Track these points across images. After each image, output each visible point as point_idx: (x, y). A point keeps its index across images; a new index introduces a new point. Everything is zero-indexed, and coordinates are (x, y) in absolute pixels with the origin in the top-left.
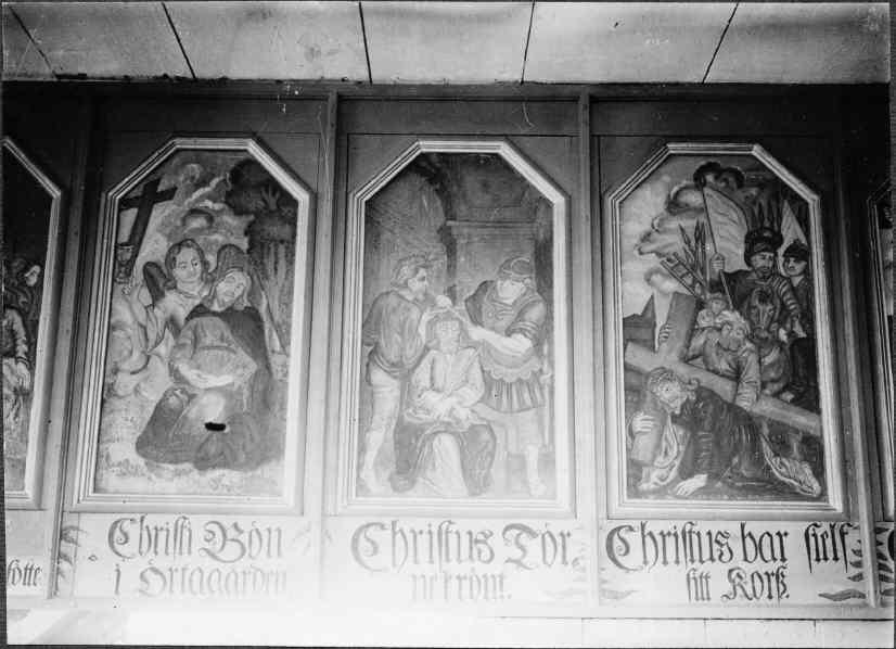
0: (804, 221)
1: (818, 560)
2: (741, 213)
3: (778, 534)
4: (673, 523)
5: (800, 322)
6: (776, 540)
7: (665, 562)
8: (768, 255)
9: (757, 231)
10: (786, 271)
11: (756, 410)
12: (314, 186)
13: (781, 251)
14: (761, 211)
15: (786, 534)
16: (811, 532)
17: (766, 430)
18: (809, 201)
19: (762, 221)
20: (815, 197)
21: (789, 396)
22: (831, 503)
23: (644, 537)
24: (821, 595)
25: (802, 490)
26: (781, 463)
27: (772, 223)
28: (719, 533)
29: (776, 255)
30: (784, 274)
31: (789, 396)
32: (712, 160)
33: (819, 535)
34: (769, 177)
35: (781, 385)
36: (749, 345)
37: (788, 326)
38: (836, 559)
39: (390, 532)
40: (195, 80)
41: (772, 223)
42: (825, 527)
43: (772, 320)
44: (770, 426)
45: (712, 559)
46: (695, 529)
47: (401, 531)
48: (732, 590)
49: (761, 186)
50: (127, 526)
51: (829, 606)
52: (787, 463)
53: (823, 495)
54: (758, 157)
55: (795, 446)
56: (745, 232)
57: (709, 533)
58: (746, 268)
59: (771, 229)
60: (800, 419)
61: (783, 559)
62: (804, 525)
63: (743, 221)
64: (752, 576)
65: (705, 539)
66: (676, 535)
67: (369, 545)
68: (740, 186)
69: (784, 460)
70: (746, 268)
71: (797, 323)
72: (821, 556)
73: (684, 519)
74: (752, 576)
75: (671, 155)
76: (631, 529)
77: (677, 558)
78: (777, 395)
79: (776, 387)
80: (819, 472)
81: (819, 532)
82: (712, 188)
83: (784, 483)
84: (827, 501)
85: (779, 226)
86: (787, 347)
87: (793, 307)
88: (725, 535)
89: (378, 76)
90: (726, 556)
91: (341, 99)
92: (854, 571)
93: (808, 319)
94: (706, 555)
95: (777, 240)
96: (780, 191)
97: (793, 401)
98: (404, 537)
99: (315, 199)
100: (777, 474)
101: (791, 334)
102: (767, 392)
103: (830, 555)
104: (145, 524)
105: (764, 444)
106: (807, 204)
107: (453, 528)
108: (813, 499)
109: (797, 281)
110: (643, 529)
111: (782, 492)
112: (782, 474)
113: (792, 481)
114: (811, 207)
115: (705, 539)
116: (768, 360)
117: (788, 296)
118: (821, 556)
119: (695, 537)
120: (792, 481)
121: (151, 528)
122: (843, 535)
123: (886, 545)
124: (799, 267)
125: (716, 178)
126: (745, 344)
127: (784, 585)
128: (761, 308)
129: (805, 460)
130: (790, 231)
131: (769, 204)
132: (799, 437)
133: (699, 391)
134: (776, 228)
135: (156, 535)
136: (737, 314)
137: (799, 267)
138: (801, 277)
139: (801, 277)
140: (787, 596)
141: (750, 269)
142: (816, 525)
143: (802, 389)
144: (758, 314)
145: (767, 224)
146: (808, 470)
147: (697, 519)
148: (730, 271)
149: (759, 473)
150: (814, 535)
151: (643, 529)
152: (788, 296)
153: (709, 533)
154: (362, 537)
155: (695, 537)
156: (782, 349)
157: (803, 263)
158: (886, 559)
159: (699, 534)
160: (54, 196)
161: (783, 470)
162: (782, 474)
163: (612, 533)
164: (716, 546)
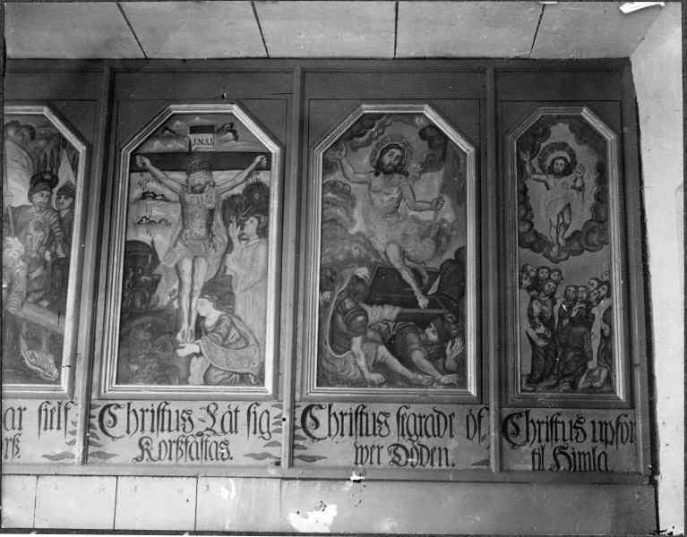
0: (75, 168)
1: (46, 429)
2: (30, 162)
3: (20, 409)
4: (150, 403)
5: (62, 246)
6: (17, 413)
7: (342, 435)
8: (46, 193)
9: (41, 175)
10: (57, 206)
11: (21, 314)
12: (283, 140)
13: (56, 190)
14: (45, 161)
15: (25, 409)
16: (44, 407)
17: (24, 330)
18: (80, 151)
19: (45, 167)
20: (84, 148)
21: (45, 303)
22: (469, 390)
23: (129, 413)
24: (44, 456)
25: (46, 376)
26: (33, 354)
27: (52, 168)
28: (381, 413)
29: (52, 193)
30: (55, 207)
31: (45, 303)
32: (15, 119)
33: (49, 410)
34: (54, 132)
35: (41, 295)
36: (21, 263)
37: (53, 248)
38: (59, 428)
39: (125, 411)
40: (146, 59)
41: (52, 168)
42: (55, 403)
43: (41, 244)
44: (28, 326)
45: (374, 434)
46: (167, 408)
47: (134, 411)
48: (554, 462)
49: (48, 139)
50: (315, 412)
51: (50, 464)
52: (37, 356)
53: (58, 381)
54: (48, 116)
55: (44, 342)
56: (31, 177)
57: (177, 411)
58: (28, 203)
59: (51, 173)
60: (48, 320)
61: (20, 428)
62: (39, 402)
63: (31, 167)
64: (160, 445)
65: (371, 417)
66: (153, 411)
67: (111, 419)
68: (33, 137)
69: (35, 352)
70: (28, 203)
71: (60, 247)
72: (233, 430)
73: (42, 398)
74: (160, 445)
75: (174, 114)
76: (118, 406)
77: (351, 431)
78: (36, 302)
79: (37, 296)
80: (58, 364)
81: (50, 407)
82: (12, 141)
83: (32, 370)
84: (60, 384)
85: (57, 172)
86: (49, 265)
87: (58, 234)
88: (386, 414)
89: (275, 52)
90: (581, 438)
91: (304, 72)
92: (70, 438)
93: (67, 242)
94: (371, 432)
95: (53, 182)
96: (64, 143)
97: (48, 307)
98: (136, 415)
99: (90, 153)
100: (27, 362)
101: (54, 255)
102: (30, 300)
103: (55, 425)
104: (332, 412)
105: (22, 341)
106: (78, 153)
107: (167, 408)
108: (51, 383)
109: (63, 214)
110: (129, 408)
111: (28, 376)
112: (31, 363)
113: (39, 369)
114: (81, 156)
115: (371, 417)
116: (34, 275)
117: (56, 225)
118: (233, 430)
119: (364, 417)
120: (39, 369)
121: (138, 410)
122: (66, 409)
123: (97, 418)
124: (67, 203)
125: (16, 132)
126: (18, 262)
127: (18, 449)
128: (35, 234)
129: (51, 352)
130: (65, 174)
131: (52, 154)
132: (49, 335)
133: (202, 296)
134: (54, 173)
135: (143, 416)
136: (16, 239)
137: (67, 203)
138: (67, 211)
139: (67, 211)
140: (19, 457)
141: (31, 204)
142: (47, 402)
143: (55, 298)
144: (31, 240)
145: (48, 169)
146: (51, 361)
147: (261, 401)
148: (15, 206)
149: (14, 363)
150: (46, 410)
151: (129, 408)
152: (56, 225)
153: (177, 411)
154: (107, 412)
155: (166, 414)
156: (45, 267)
157: (71, 200)
158: (96, 429)
159: (367, 415)
160: (273, 152)
161: (33, 360)
162: (31, 363)
163: (103, 411)
164: (377, 424)
